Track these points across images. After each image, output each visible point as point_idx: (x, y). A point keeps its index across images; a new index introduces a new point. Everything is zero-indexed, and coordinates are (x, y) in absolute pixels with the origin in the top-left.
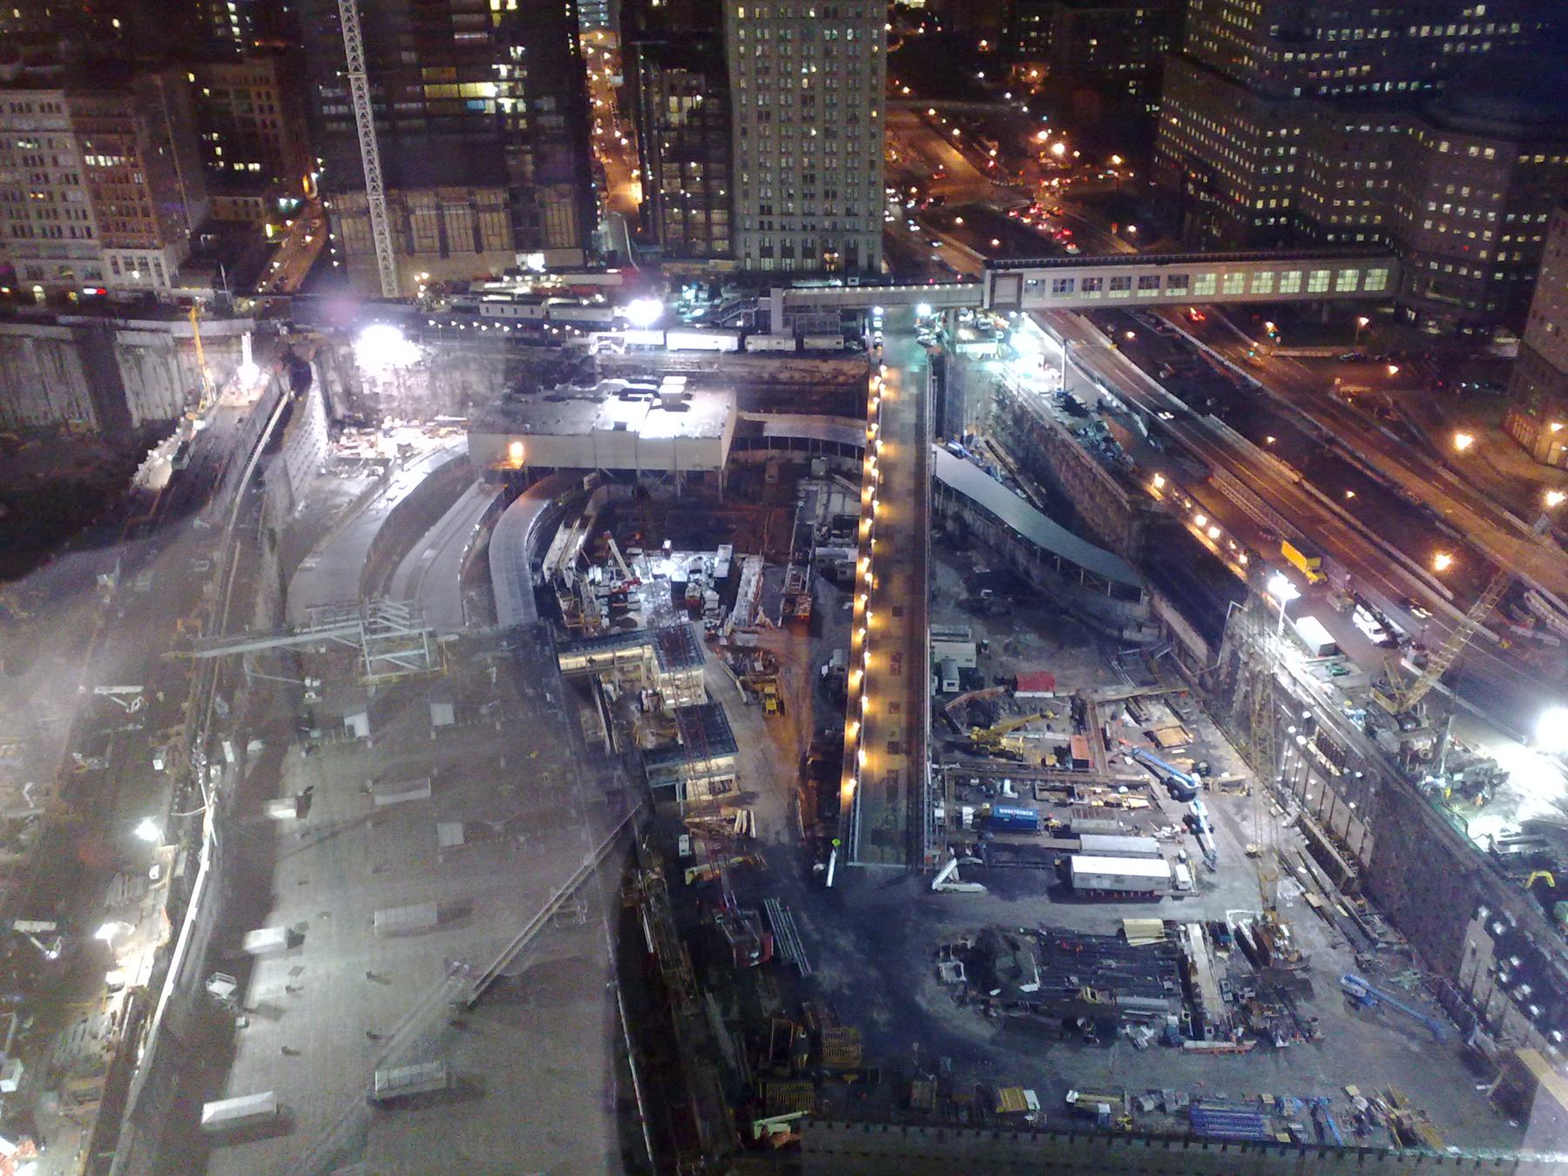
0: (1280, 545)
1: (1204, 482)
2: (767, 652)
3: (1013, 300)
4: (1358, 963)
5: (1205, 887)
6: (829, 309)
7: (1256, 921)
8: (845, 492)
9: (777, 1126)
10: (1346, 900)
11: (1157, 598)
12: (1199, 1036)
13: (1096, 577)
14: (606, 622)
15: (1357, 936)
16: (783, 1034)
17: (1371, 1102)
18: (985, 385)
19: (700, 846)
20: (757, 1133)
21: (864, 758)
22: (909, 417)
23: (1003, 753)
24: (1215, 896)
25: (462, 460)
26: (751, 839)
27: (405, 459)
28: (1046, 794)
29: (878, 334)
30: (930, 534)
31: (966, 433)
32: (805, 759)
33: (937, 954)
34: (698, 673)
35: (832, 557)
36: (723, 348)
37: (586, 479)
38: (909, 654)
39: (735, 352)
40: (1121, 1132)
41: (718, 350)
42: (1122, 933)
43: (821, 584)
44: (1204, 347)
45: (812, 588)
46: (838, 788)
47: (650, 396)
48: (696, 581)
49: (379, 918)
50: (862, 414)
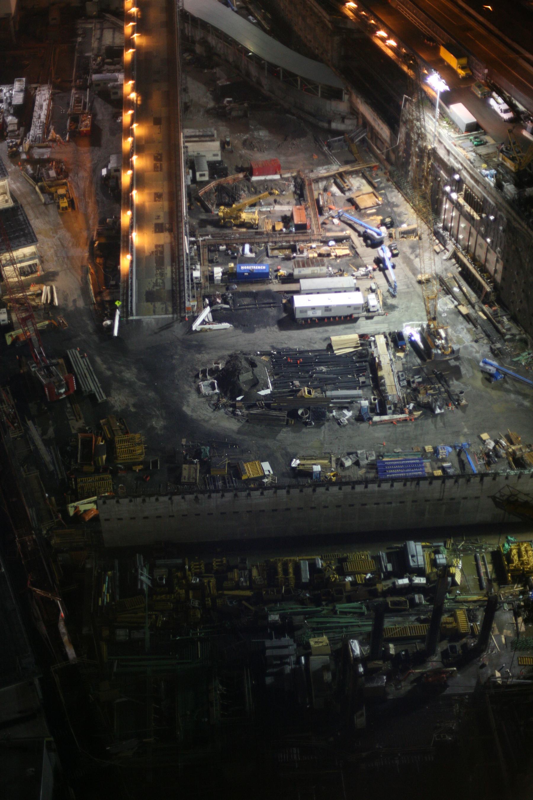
2: (59, 162)
4: (492, 350)
5: (389, 308)
7: (423, 329)
9: (87, 506)
10: (485, 308)
11: (354, 96)
12: (383, 412)
13: (309, 81)
15: (491, 331)
16: (87, 443)
17: (497, 442)
20: (72, 512)
23: (243, 225)
24: (395, 314)
28: (276, 252)
33: (197, 376)
35: (106, 81)
38: (167, 154)
40: (329, 483)
42: (330, 347)
45: (91, 108)
46: (118, 263)
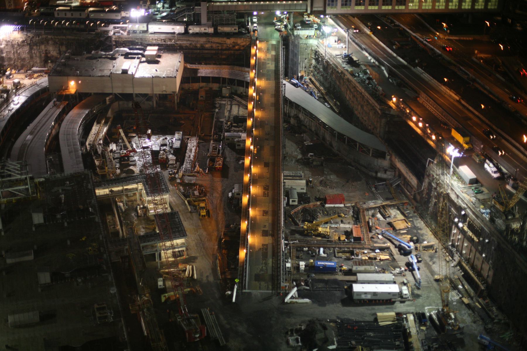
0: (451, 131)
1: (415, 100)
2: (201, 186)
3: (322, 9)
4: (486, 329)
6: (230, 12)
7: (439, 312)
8: (239, 105)
11: (393, 157)
13: (363, 145)
14: (118, 171)
18: (309, 51)
19: (169, 284)
21: (251, 239)
22: (271, 66)
23: (319, 235)
24: (420, 301)
25: (44, 90)
26: (194, 279)
27: (17, 90)
28: (340, 254)
29: (255, 25)
30: (283, 125)
31: (300, 75)
32: (221, 240)
33: (287, 333)
34: (166, 197)
35: (233, 137)
36: (177, 32)
37: (107, 99)
38: (273, 186)
39: (183, 34)
41: (174, 33)
42: (376, 320)
43: (228, 151)
44: (414, 34)
45: (223, 153)
46: (238, 254)
47: (140, 56)
48: (164, 150)
49: (11, 319)
50: (248, 65)
